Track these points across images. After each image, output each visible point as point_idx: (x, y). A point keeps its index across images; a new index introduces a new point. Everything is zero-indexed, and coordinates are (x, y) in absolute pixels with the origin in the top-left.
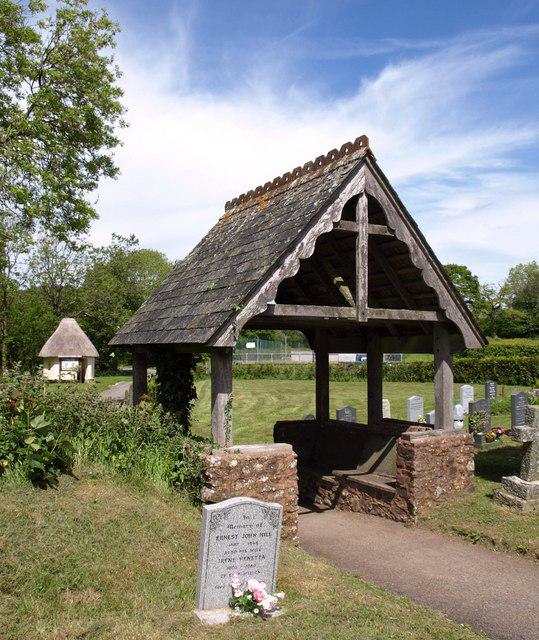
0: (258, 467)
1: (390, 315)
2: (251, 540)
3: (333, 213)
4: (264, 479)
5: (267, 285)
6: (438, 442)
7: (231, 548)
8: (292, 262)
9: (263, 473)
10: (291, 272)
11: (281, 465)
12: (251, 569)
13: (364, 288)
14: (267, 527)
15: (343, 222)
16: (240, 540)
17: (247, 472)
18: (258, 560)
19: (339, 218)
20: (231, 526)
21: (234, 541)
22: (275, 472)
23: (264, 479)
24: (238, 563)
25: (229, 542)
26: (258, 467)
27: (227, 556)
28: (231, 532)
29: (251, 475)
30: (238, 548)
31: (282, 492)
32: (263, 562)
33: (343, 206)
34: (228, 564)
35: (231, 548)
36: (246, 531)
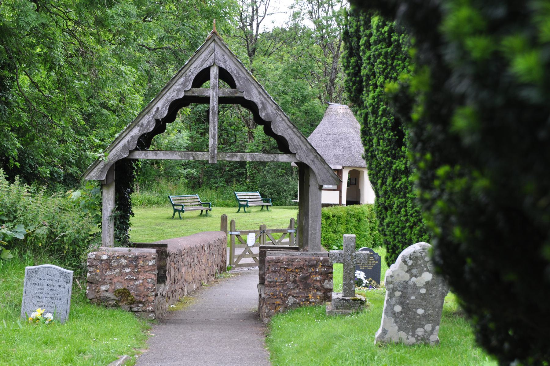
0: (124, 262)
1: (242, 157)
2: (52, 288)
3: (184, 84)
4: (128, 270)
5: (128, 138)
6: (292, 260)
7: (40, 291)
8: (149, 122)
9: (127, 266)
10: (148, 129)
11: (141, 263)
12: (52, 305)
13: (214, 137)
14: (62, 283)
15: (194, 89)
16: (45, 287)
17: (114, 264)
18: (56, 300)
19: (190, 87)
20: (39, 279)
21: (41, 287)
22: (136, 266)
23: (128, 270)
24: (44, 299)
25: (39, 287)
26: (124, 262)
27: (37, 295)
28: (39, 282)
29: (118, 266)
30: (44, 291)
31: (141, 281)
32: (60, 302)
33: (193, 77)
34: (38, 299)
35: (40, 291)
36: (49, 282)
